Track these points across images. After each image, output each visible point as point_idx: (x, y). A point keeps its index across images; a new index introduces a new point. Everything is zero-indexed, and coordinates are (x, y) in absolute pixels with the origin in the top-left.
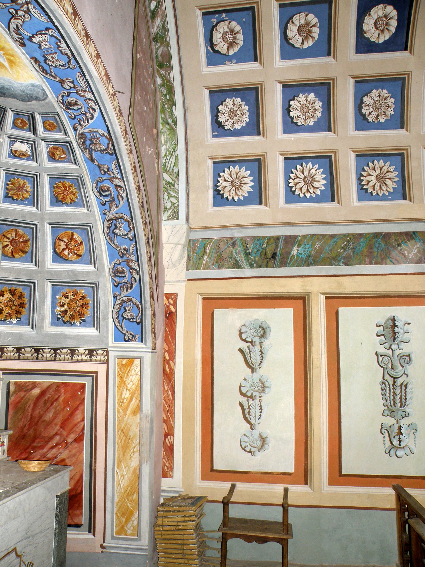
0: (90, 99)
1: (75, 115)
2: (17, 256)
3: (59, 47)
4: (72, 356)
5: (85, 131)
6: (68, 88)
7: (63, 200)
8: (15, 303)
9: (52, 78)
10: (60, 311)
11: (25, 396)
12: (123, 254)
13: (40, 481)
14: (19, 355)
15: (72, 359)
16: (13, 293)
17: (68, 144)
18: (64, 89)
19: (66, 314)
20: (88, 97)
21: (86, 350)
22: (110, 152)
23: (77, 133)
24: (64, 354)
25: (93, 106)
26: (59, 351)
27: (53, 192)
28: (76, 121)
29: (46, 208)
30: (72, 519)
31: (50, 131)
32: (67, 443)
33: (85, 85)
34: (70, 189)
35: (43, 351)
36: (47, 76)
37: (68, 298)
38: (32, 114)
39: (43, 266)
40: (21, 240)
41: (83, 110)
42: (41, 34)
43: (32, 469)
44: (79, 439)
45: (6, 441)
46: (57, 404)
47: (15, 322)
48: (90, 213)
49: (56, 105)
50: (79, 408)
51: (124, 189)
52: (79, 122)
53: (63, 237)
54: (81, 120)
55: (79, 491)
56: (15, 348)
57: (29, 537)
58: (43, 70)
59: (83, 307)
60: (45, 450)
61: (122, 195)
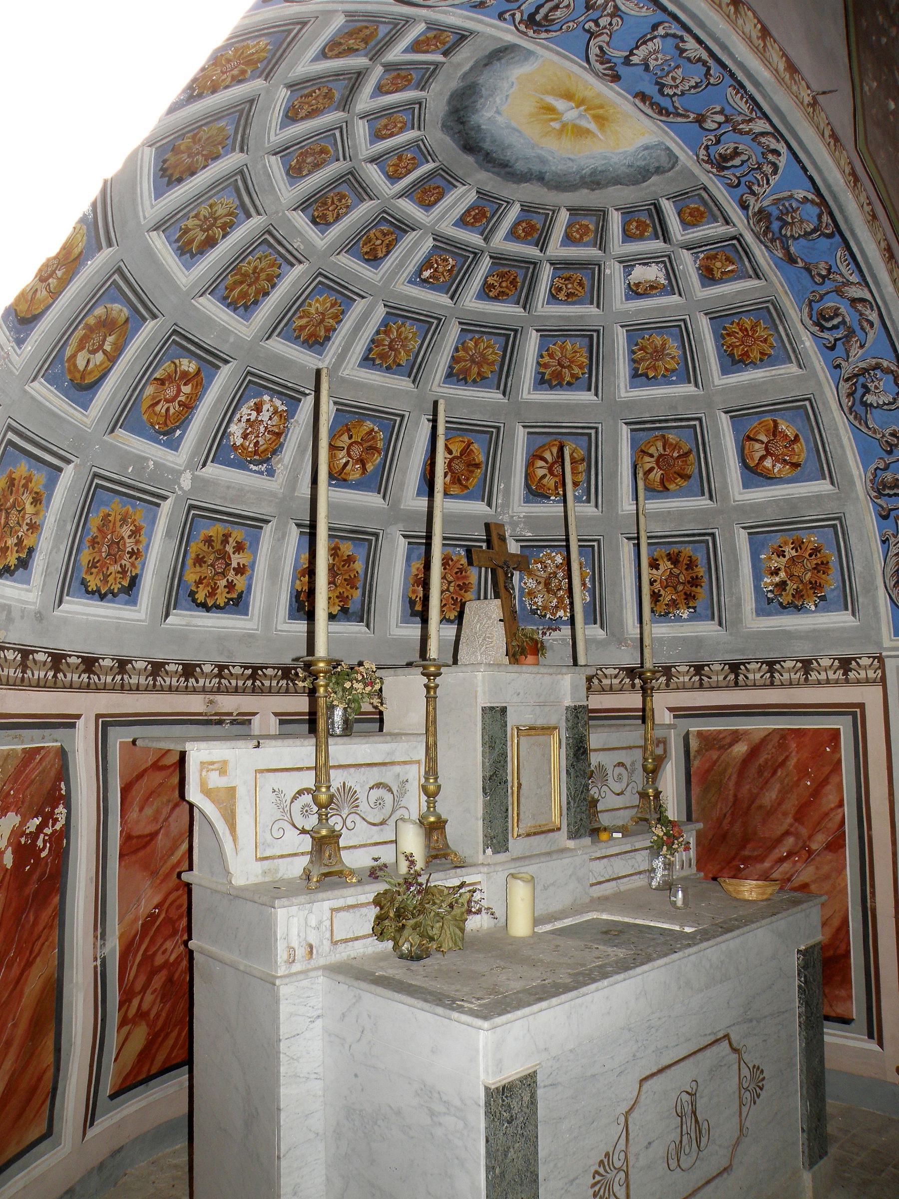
0: (763, 134)
1: (738, 178)
2: (672, 487)
3: (683, 51)
4: (807, 673)
5: (766, 203)
6: (715, 126)
7: (745, 358)
8: (682, 578)
9: (679, 120)
10: (771, 584)
11: (719, 758)
12: (891, 445)
13: (763, 918)
14: (701, 679)
15: (806, 679)
16: (674, 559)
17: (735, 242)
18: (707, 133)
19: (785, 590)
20: (757, 130)
21: (835, 659)
22: (827, 231)
23: (750, 212)
24: (789, 671)
25: (774, 144)
26: (778, 667)
27: (723, 345)
28: (743, 189)
29: (713, 382)
30: (831, 1006)
31: (694, 225)
32: (810, 852)
33: (748, 108)
34: (755, 332)
35: (746, 667)
36: (671, 119)
37: (784, 556)
38: (654, 204)
39: (726, 497)
40: (676, 455)
41: (754, 160)
42: (645, 43)
43: (747, 896)
44: (836, 844)
45: (692, 841)
46: (785, 774)
47: (685, 616)
48: (804, 372)
49: (696, 170)
50: (830, 780)
51: (871, 303)
52: (750, 188)
53: (757, 433)
54: (753, 184)
55: (841, 951)
56: (690, 666)
57: (751, 1021)
58: (662, 111)
59: (819, 572)
60: (767, 865)
61: (870, 318)
